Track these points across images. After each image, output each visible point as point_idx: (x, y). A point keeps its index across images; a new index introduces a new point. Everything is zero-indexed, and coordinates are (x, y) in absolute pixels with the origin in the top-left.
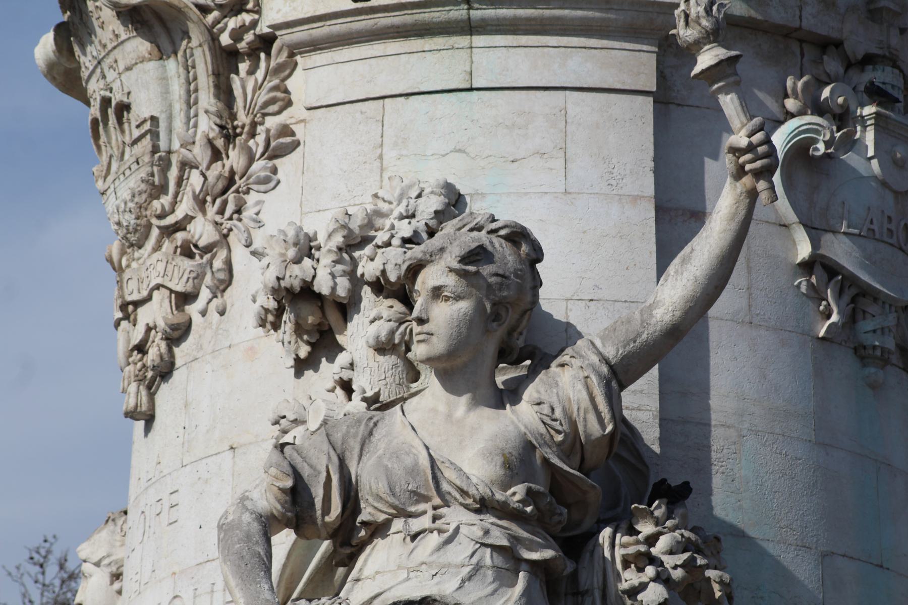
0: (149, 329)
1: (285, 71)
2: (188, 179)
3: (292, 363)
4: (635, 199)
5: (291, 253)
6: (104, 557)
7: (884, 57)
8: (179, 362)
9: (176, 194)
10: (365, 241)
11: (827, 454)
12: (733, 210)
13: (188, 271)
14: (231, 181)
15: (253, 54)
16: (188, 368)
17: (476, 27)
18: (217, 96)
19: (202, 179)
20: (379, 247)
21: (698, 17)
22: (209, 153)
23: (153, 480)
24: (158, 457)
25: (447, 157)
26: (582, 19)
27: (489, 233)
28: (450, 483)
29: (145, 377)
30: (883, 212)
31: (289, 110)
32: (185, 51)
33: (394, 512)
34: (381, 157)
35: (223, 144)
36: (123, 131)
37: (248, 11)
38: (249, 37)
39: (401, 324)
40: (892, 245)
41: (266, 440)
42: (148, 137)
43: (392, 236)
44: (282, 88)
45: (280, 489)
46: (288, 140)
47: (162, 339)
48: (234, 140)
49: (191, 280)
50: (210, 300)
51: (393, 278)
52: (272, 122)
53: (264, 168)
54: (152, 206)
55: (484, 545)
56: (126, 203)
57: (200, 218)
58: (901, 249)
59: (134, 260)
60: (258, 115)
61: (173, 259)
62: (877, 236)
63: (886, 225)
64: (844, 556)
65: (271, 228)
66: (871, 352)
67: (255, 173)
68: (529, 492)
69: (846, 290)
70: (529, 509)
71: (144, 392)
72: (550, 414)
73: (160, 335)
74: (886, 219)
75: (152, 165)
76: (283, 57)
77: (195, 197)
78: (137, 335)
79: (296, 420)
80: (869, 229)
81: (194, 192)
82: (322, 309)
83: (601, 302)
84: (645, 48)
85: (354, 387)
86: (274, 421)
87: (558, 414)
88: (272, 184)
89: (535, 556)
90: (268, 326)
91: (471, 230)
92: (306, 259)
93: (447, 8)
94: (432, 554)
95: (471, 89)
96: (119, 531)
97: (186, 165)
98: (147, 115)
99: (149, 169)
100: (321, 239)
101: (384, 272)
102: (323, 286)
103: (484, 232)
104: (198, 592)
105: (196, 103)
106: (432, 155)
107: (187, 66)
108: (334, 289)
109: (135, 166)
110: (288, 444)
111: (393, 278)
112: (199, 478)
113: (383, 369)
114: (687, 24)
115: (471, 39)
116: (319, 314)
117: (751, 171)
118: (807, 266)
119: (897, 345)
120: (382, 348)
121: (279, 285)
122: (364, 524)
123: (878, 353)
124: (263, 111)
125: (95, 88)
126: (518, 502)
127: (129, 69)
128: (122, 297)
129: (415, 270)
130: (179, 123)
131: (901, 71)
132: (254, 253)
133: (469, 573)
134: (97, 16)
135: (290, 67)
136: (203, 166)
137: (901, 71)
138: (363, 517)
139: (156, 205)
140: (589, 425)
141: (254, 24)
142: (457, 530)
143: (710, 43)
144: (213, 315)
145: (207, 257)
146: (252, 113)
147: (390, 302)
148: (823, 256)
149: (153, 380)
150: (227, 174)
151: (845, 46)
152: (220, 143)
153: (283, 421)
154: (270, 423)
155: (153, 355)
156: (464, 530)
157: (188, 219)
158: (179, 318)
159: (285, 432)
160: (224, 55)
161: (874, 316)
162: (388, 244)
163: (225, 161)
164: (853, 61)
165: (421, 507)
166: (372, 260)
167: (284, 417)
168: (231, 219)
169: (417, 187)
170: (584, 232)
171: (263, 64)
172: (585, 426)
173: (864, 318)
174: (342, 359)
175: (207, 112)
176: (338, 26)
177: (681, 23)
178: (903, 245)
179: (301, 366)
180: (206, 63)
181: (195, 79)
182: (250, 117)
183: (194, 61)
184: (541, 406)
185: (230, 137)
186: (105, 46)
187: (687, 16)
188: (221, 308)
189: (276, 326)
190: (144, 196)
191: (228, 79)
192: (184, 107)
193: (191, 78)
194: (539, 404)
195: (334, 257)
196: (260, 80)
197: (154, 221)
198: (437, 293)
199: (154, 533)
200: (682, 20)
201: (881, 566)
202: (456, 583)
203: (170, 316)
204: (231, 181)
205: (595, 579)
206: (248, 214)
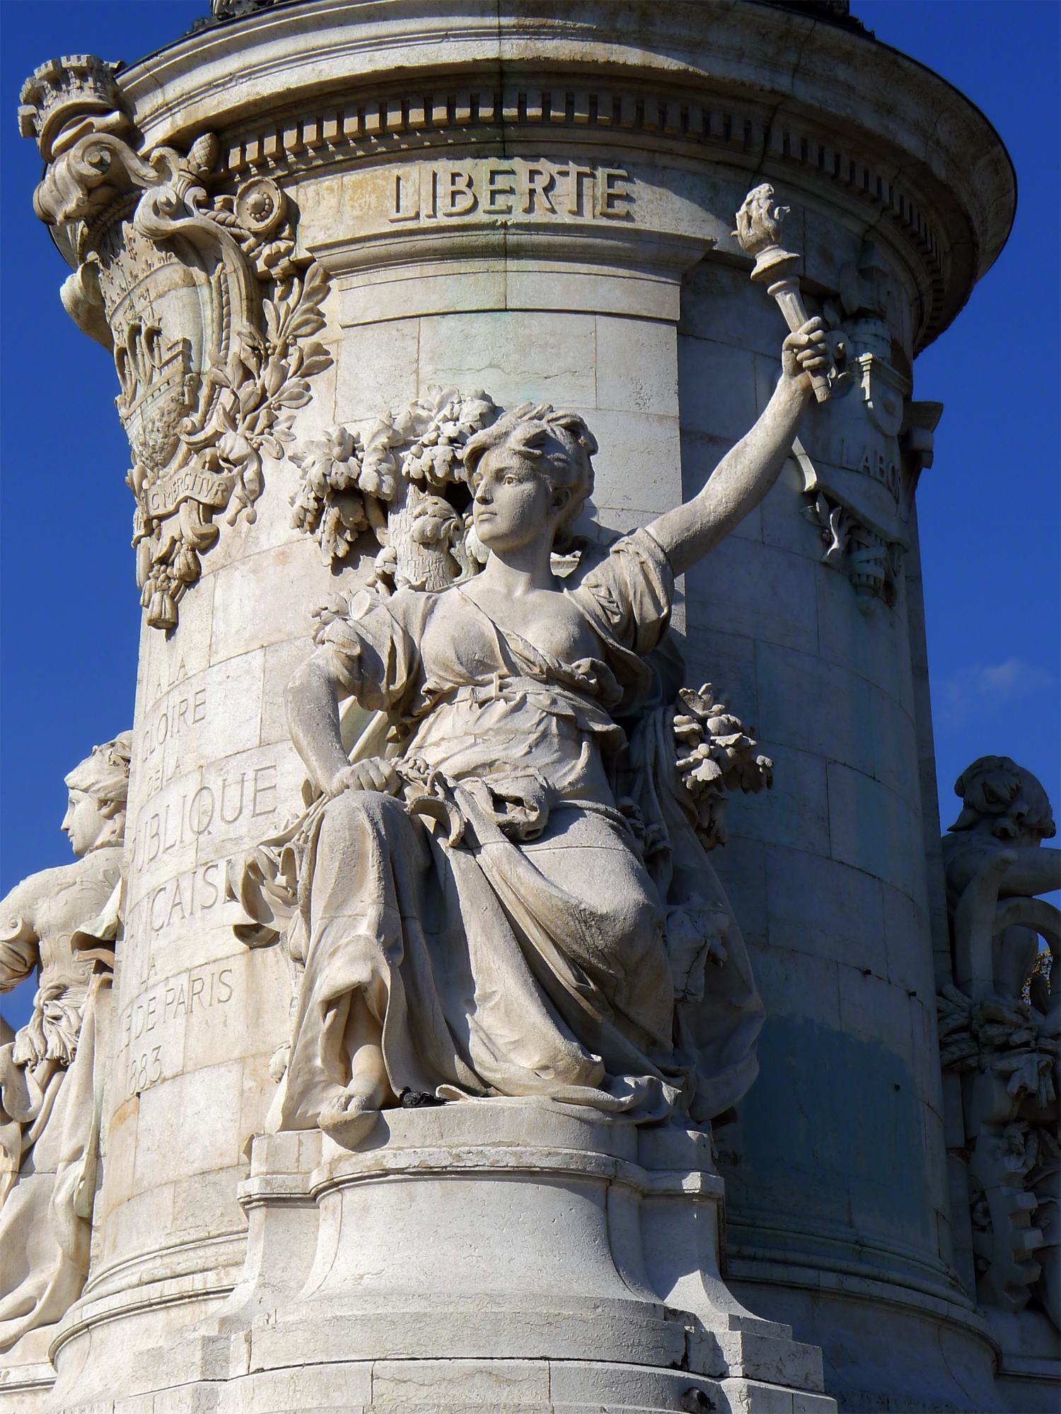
0: (174, 542)
1: (318, 295)
2: (218, 398)
3: (330, 561)
4: (662, 418)
5: (337, 451)
6: (93, 784)
7: (874, 312)
9: (206, 412)
10: (406, 445)
12: (788, 407)
14: (263, 398)
15: (287, 279)
16: (214, 576)
17: (512, 252)
18: (250, 319)
20: (426, 446)
21: (761, 218)
22: (241, 372)
23: (177, 683)
24: (182, 661)
25: (483, 371)
26: (611, 248)
27: (549, 422)
28: (516, 653)
29: (169, 587)
30: (876, 452)
32: (219, 277)
33: (461, 680)
34: (417, 372)
35: (255, 363)
36: (153, 357)
38: (284, 262)
39: (445, 520)
40: (881, 483)
41: (299, 638)
42: (180, 358)
43: (439, 436)
44: (315, 311)
45: (347, 656)
46: (322, 358)
47: (188, 550)
49: (219, 493)
53: (297, 385)
54: (182, 424)
55: (550, 714)
57: (230, 432)
58: (889, 489)
59: (159, 478)
60: (290, 337)
63: (879, 465)
64: (844, 765)
67: (288, 389)
68: (593, 665)
70: (592, 681)
71: (168, 602)
72: (608, 596)
76: (317, 282)
77: (226, 414)
78: (160, 549)
79: (338, 611)
81: (224, 409)
82: (364, 507)
83: (631, 512)
84: (669, 281)
86: (315, 613)
87: (615, 596)
88: (306, 399)
89: (598, 727)
90: (307, 526)
92: (351, 458)
93: (485, 232)
94: (499, 720)
95: (506, 310)
96: (107, 760)
97: (216, 386)
98: (179, 337)
99: (179, 389)
100: (364, 441)
101: (432, 469)
102: (368, 482)
103: (544, 420)
104: (227, 783)
105: (228, 326)
106: (468, 370)
107: (221, 291)
108: (380, 485)
112: (228, 677)
113: (427, 563)
115: (506, 263)
116: (361, 513)
117: (809, 368)
118: (812, 495)
120: (428, 542)
122: (429, 692)
124: (294, 333)
126: (583, 674)
127: (161, 296)
128: (148, 512)
130: (209, 346)
133: (536, 739)
134: (130, 248)
135: (323, 290)
136: (234, 386)
138: (429, 685)
139: (187, 422)
140: (645, 608)
141: (289, 251)
142: (524, 699)
143: (772, 243)
145: (236, 470)
146: (284, 335)
147: (435, 499)
149: (178, 588)
150: (259, 392)
151: (842, 298)
152: (252, 363)
153: (324, 613)
156: (530, 699)
157: (218, 435)
158: (206, 529)
161: (868, 547)
163: (257, 381)
164: (848, 312)
165: (487, 677)
166: (419, 458)
167: (326, 608)
168: (262, 433)
169: (456, 396)
170: (614, 446)
171: (296, 289)
172: (641, 609)
173: (859, 549)
174: (383, 554)
175: (239, 334)
179: (338, 565)
181: (228, 303)
182: (282, 339)
183: (227, 287)
184: (598, 589)
185: (262, 359)
186: (136, 277)
187: (750, 218)
188: (251, 518)
190: (173, 415)
192: (216, 329)
194: (596, 586)
195: (379, 455)
197: (184, 438)
199: (178, 732)
200: (745, 221)
201: (874, 778)
202: (523, 749)
203: (198, 526)
204: (263, 398)
206: (280, 428)
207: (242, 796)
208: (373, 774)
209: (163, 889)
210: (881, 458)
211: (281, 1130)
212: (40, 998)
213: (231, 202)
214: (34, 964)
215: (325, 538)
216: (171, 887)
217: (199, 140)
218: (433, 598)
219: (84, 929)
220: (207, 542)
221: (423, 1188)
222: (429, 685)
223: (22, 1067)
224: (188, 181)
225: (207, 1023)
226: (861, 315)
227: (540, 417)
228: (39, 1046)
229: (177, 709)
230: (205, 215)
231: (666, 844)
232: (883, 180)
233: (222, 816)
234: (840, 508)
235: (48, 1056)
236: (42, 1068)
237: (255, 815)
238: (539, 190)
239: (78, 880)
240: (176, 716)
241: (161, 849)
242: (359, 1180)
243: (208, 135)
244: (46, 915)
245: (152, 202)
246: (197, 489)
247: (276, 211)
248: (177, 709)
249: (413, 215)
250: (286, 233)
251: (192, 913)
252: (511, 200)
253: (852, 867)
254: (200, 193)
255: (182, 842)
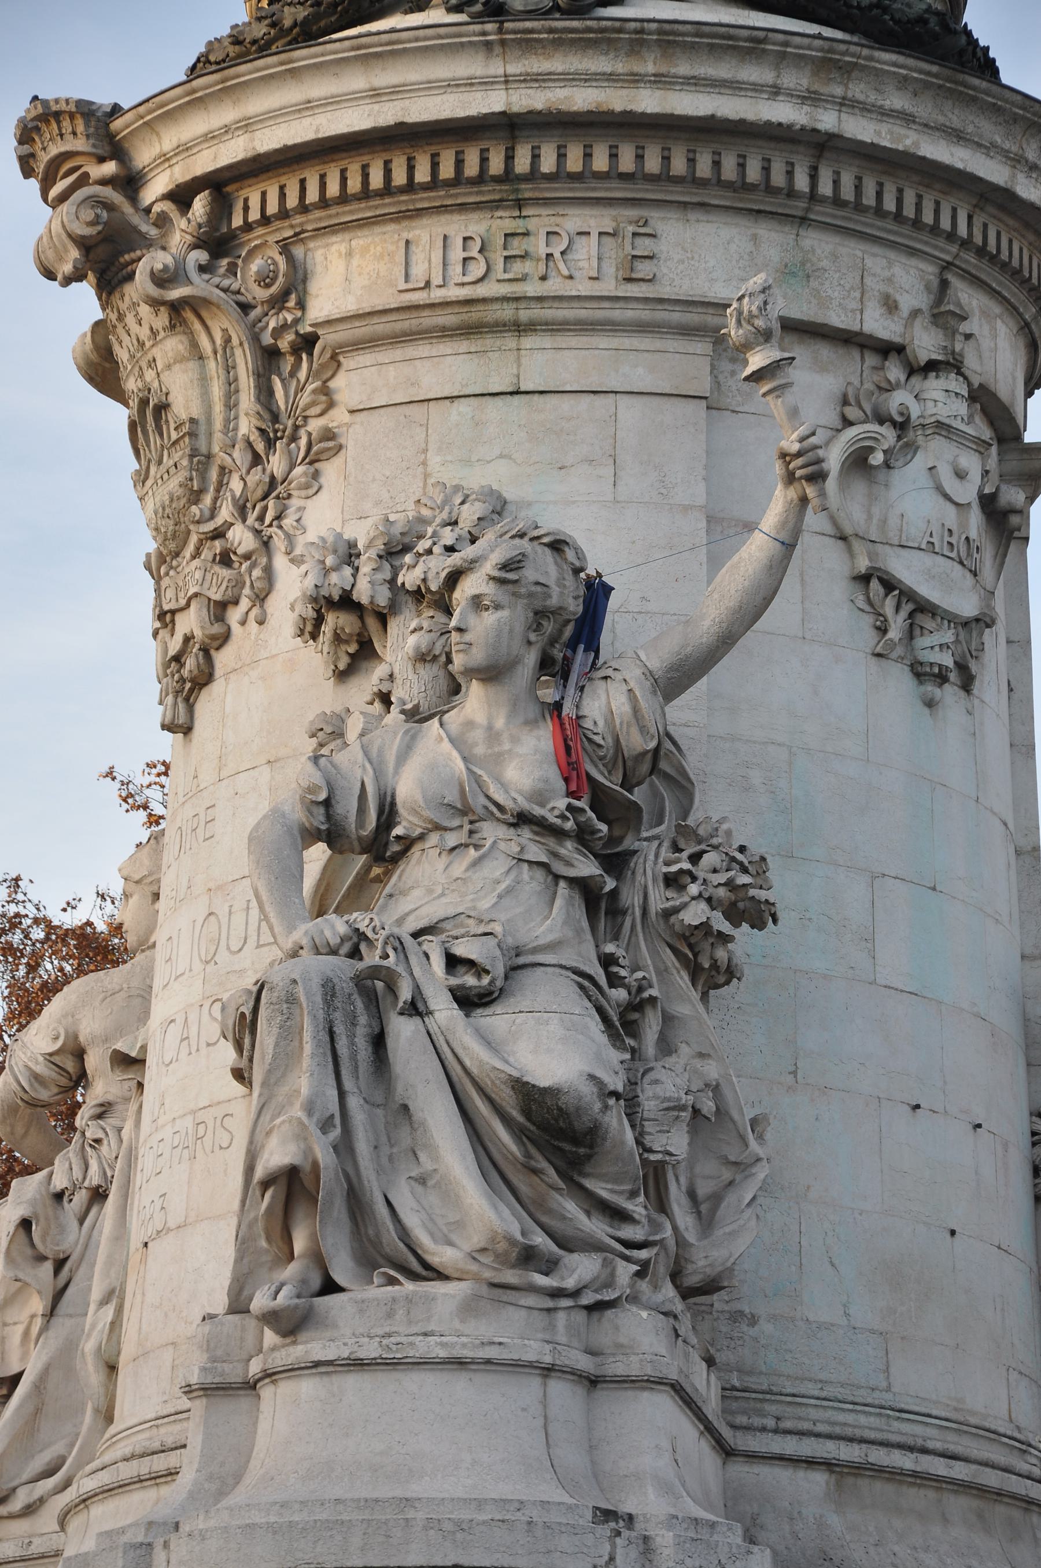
7: (948, 363)
8: (219, 671)
10: (406, 549)
11: (881, 773)
13: (226, 579)
19: (242, 483)
22: (249, 457)
23: (190, 794)
30: (943, 525)
31: (332, 413)
34: (424, 463)
36: (161, 435)
37: (288, 310)
48: (275, 444)
50: (250, 610)
51: (434, 588)
52: (315, 425)
53: (305, 474)
56: (164, 509)
58: (961, 563)
61: (211, 567)
62: (937, 550)
63: (947, 539)
65: (311, 536)
66: (928, 669)
69: (903, 605)
71: (181, 706)
73: (197, 646)
74: (946, 533)
75: (191, 470)
80: (928, 542)
82: (361, 618)
85: (393, 699)
90: (307, 636)
91: (513, 537)
95: (517, 393)
99: (187, 474)
101: (424, 580)
102: (363, 593)
103: (526, 538)
105: (236, 405)
106: (478, 461)
109: (173, 470)
110: (323, 756)
111: (434, 588)
114: (739, 322)
117: (801, 478)
119: (955, 662)
120: (423, 658)
121: (318, 593)
123: (936, 670)
125: (131, 385)
129: (454, 578)
131: (965, 378)
132: (292, 561)
137: (965, 378)
141: (297, 321)
144: (252, 625)
148: (879, 569)
149: (191, 690)
150: (267, 480)
152: (260, 447)
153: (320, 734)
154: (306, 736)
155: (190, 663)
156: (502, 845)
159: (321, 745)
160: (266, 355)
162: (429, 552)
164: (915, 366)
167: (322, 729)
168: (270, 525)
171: (305, 365)
173: (922, 635)
174: (380, 671)
175: (247, 414)
176: (382, 325)
177: (732, 323)
178: (963, 559)
179: (343, 675)
180: (246, 363)
181: (236, 380)
183: (234, 361)
189: (314, 636)
190: (183, 501)
191: (269, 380)
193: (231, 380)
196: (303, 379)
198: (477, 602)
201: (934, 889)
205: (636, 898)
207: (247, 924)
208: (328, 934)
209: (172, 1021)
210: (950, 530)
211: (227, 1314)
212: (82, 1119)
213: (236, 265)
214: (81, 1078)
215: (326, 649)
216: (180, 1021)
217: (198, 197)
218: (413, 731)
219: (121, 1046)
220: (218, 642)
221: (352, 1382)
222: (398, 831)
223: (59, 1196)
224: (188, 242)
225: (209, 1171)
226: (932, 367)
227: (521, 535)
228: (77, 1173)
229: (190, 823)
230: (208, 281)
231: (654, 992)
232: (959, 211)
233: (228, 945)
234: (897, 592)
235: (86, 1184)
236: (81, 1197)
237: (259, 946)
238: (557, 255)
239: (125, 986)
240: (189, 832)
241: (173, 977)
242: (292, 1371)
243: (207, 192)
244: (89, 1028)
245: (148, 269)
246: (206, 585)
247: (281, 279)
248: (190, 823)
249: (422, 285)
250: (291, 303)
251: (198, 1050)
252: (527, 267)
253: (902, 991)
254: (201, 256)
255: (191, 970)
